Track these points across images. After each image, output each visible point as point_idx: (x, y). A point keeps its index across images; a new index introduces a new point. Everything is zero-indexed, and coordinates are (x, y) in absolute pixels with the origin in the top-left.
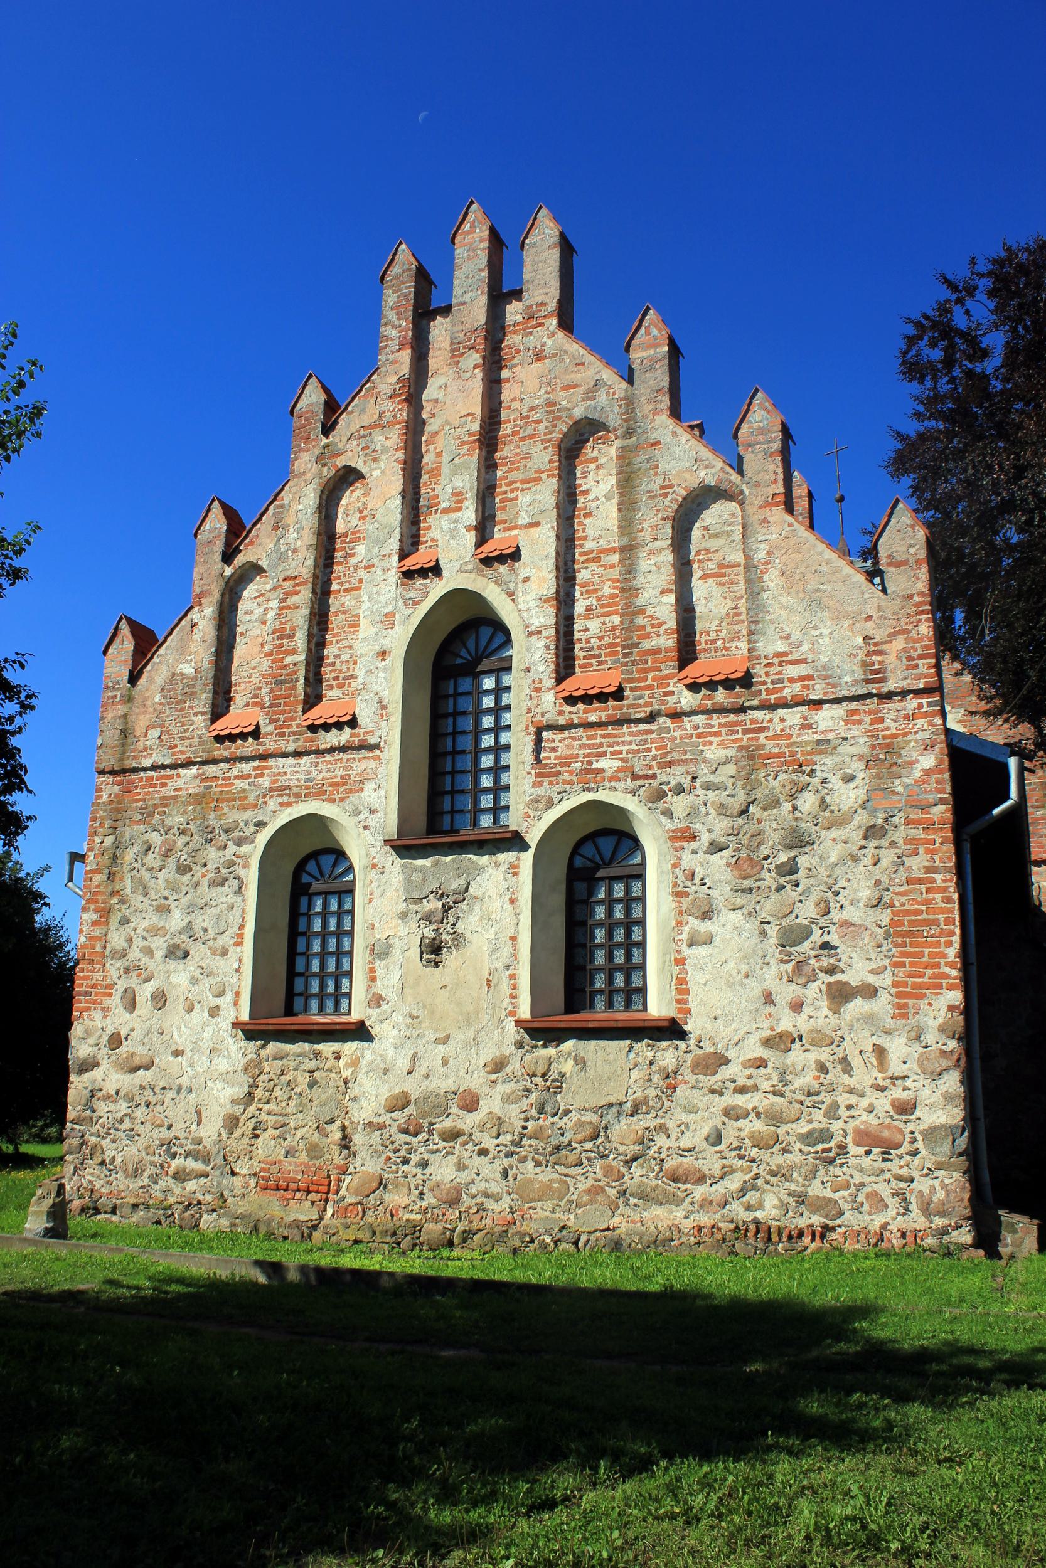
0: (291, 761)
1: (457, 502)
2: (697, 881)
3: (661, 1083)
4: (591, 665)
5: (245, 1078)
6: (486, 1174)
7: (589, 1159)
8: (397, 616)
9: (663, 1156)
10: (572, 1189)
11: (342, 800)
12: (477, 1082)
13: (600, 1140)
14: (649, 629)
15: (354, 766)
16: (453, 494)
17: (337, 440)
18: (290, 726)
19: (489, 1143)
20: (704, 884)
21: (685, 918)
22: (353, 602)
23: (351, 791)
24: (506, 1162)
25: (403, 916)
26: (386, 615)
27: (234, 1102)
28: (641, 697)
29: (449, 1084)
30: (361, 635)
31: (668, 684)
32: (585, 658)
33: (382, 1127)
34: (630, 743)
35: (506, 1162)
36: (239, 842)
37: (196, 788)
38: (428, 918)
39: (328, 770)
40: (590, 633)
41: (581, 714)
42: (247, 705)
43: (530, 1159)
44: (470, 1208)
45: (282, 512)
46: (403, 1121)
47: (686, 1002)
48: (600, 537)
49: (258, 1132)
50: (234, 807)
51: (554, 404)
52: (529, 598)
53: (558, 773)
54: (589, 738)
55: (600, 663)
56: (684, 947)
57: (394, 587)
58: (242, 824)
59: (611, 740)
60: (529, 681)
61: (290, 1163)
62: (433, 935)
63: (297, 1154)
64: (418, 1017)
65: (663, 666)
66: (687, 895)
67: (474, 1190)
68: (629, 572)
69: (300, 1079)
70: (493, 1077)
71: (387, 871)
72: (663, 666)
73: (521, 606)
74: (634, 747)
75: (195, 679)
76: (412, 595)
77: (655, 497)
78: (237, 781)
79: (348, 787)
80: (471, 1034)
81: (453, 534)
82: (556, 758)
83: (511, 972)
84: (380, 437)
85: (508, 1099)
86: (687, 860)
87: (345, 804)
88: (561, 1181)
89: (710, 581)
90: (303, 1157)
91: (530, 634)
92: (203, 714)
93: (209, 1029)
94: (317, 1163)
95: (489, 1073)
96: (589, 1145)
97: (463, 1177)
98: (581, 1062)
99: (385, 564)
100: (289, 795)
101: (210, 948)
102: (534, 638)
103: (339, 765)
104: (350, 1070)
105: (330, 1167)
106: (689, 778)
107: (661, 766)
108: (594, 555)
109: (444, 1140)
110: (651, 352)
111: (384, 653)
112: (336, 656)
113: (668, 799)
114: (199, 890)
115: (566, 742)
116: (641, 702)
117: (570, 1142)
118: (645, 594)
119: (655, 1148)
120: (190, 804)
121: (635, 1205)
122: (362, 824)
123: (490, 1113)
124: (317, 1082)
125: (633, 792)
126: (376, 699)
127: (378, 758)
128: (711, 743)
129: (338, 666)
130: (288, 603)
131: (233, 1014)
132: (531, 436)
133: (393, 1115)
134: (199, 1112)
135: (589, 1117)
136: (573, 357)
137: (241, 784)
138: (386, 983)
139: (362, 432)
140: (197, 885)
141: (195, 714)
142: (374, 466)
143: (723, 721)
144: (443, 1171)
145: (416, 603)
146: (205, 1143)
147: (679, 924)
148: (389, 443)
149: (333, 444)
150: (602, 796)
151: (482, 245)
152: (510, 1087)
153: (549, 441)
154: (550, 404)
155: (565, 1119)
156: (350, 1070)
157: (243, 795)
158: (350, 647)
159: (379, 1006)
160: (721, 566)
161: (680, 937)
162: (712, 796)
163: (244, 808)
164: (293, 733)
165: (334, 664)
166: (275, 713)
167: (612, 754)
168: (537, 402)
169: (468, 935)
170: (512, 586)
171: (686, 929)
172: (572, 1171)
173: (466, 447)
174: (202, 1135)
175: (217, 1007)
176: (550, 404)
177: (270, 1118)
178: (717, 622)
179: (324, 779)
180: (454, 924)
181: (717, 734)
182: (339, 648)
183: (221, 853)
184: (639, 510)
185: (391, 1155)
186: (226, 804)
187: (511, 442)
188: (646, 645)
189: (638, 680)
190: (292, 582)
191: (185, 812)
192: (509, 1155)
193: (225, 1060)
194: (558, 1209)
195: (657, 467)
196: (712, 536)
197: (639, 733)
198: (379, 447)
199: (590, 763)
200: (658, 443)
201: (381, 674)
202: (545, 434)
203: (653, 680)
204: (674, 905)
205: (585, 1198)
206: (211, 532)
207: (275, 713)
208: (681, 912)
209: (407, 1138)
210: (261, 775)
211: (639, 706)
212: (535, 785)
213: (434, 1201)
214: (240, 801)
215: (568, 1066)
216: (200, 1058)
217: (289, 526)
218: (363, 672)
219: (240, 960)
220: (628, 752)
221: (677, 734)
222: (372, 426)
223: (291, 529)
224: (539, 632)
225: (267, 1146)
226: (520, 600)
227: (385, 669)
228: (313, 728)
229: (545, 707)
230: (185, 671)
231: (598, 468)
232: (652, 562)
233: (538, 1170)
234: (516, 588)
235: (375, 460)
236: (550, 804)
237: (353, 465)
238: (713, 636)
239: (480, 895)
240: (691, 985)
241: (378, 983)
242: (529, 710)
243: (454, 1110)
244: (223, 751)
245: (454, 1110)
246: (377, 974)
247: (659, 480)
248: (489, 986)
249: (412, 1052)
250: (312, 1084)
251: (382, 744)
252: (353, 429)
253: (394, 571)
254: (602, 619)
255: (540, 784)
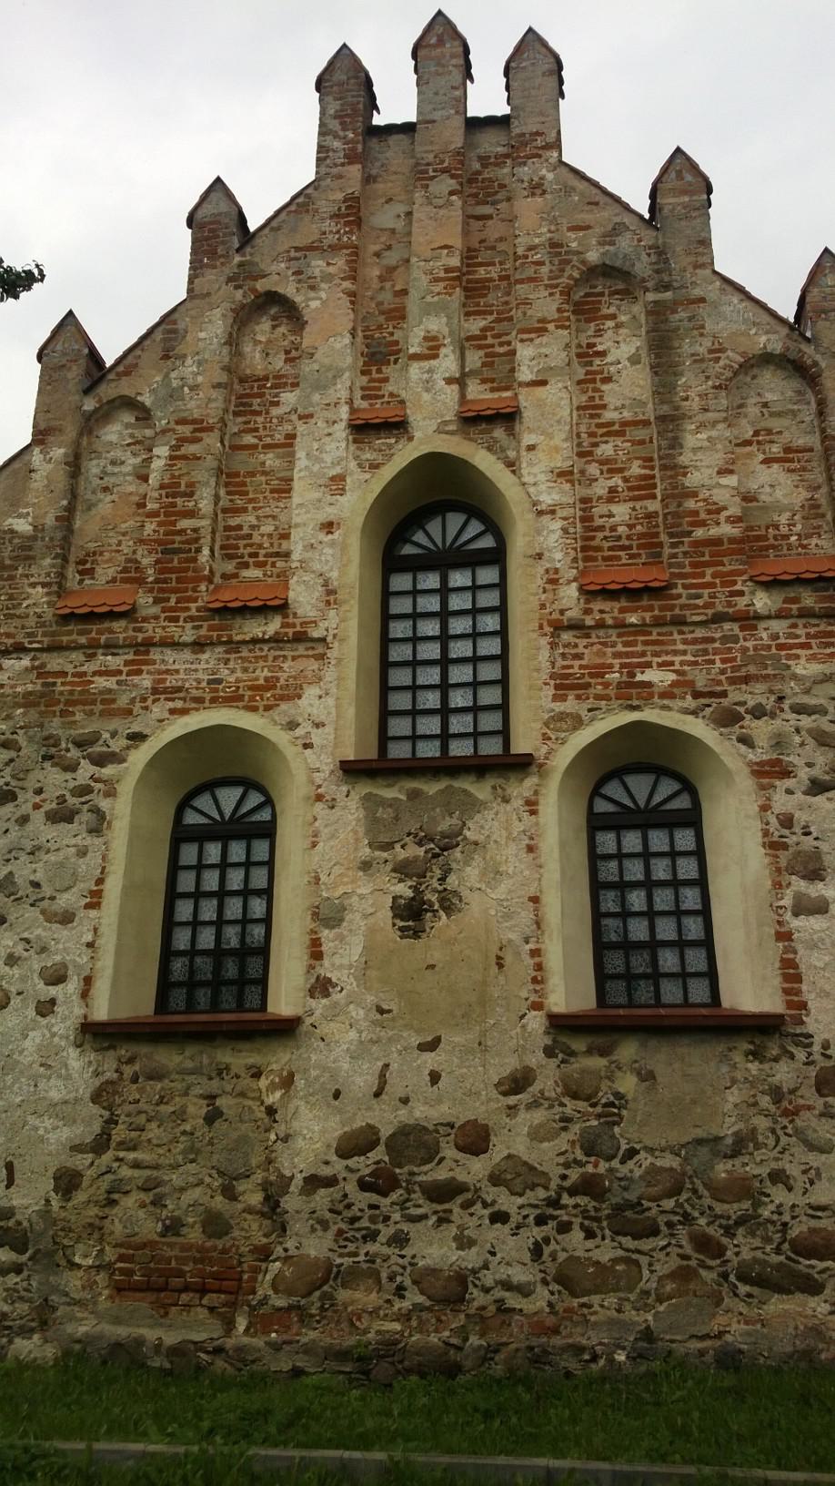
0: (187, 655)
1: (430, 348)
2: (797, 829)
3: (773, 1108)
4: (619, 558)
5: (96, 1110)
6: (508, 1257)
7: (670, 1225)
8: (348, 480)
9: (786, 1218)
10: (646, 1273)
11: (268, 708)
12: (486, 1106)
13: (684, 1196)
14: (703, 516)
15: (285, 666)
16: (425, 339)
17: (257, 259)
18: (188, 609)
19: (507, 1202)
20: (808, 834)
21: (786, 878)
22: (277, 463)
23: (282, 698)
24: (538, 1233)
25: (366, 866)
26: (333, 479)
27: (77, 1149)
28: (699, 597)
29: (443, 1112)
30: (296, 499)
31: (735, 583)
32: (610, 549)
33: (331, 1182)
34: (684, 653)
35: (538, 1233)
36: (100, 761)
37: (32, 686)
38: (403, 870)
39: (245, 670)
40: (617, 519)
41: (616, 614)
42: (114, 580)
43: (576, 1227)
44: (483, 1308)
45: (175, 339)
46: (367, 1171)
47: (798, 992)
48: (623, 406)
49: (115, 1196)
50: (91, 713)
51: (561, 246)
52: (535, 470)
53: (588, 686)
54: (626, 644)
55: (631, 557)
56: (788, 916)
57: (343, 445)
58: (106, 735)
59: (657, 648)
60: (541, 571)
61: (171, 1245)
62: (410, 893)
63: (184, 1230)
64: (389, 1011)
65: (725, 560)
66: (785, 847)
67: (488, 1278)
68: (672, 447)
69: (191, 1109)
70: (512, 1100)
71: (340, 804)
72: (725, 560)
73: (526, 479)
74: (689, 658)
75: (34, 538)
76: (368, 456)
77: (702, 360)
78: (96, 678)
79: (278, 691)
80: (472, 1036)
81: (428, 385)
82: (581, 667)
83: (531, 946)
84: (320, 262)
85: (536, 1135)
86: (781, 802)
87: (275, 714)
88: (627, 1261)
89: (776, 466)
90: (194, 1235)
91: (540, 513)
92: (44, 585)
93: (35, 1037)
94: (220, 1244)
95: (505, 1094)
96: (669, 1204)
97: (471, 1258)
98: (647, 1077)
99: (330, 415)
100: (184, 699)
101: (43, 912)
102: (546, 519)
103: (262, 663)
104: (278, 1094)
105: (244, 1249)
106: (773, 698)
107: (732, 681)
108: (616, 427)
109: (432, 1200)
110: (686, 199)
111: (330, 524)
112: (253, 527)
113: (746, 723)
114: (30, 827)
115: (595, 648)
116: (700, 602)
117: (640, 1198)
118: (697, 474)
119: (772, 1207)
120: (18, 705)
121: (749, 1295)
122: (300, 742)
123: (509, 1157)
124: (221, 1114)
125: (694, 713)
126: (321, 581)
127: (321, 657)
128: (798, 657)
129: (256, 539)
130: (183, 451)
131: (78, 1011)
132: (531, 280)
133: (350, 1162)
134: (10, 1167)
135: (669, 1161)
136: (582, 195)
137: (102, 683)
138: (337, 960)
139: (293, 254)
140: (24, 820)
141: (33, 585)
142: (312, 294)
143: (812, 631)
144: (435, 1250)
145: (375, 466)
146: (18, 1217)
147: (778, 885)
148: (331, 269)
149: (250, 263)
150: (650, 715)
151: (454, 61)
152: (539, 1116)
153: (556, 286)
154: (554, 245)
155: (631, 1164)
156: (278, 1094)
157: (108, 698)
158: (274, 517)
159: (327, 995)
160: (787, 450)
161: (781, 903)
162: (806, 721)
163: (108, 714)
164: (192, 619)
165: (250, 536)
166: (161, 590)
167: (659, 665)
168: (537, 241)
169: (465, 893)
170: (512, 454)
171: (789, 893)
172: (646, 1244)
173: (442, 284)
174: (14, 1203)
175: (53, 1002)
176: (554, 245)
177: (137, 1173)
178: (788, 514)
179: (238, 681)
180: (442, 880)
181: (807, 646)
182: (258, 518)
183: (69, 776)
184: (682, 375)
185: (344, 1226)
186: (80, 707)
187: (497, 287)
188: (699, 533)
189: (694, 576)
190: (191, 427)
191: (8, 717)
192: (541, 1221)
193: (60, 1083)
194: (627, 1306)
195: (703, 327)
196: (772, 415)
197: (695, 641)
198: (317, 272)
199: (632, 675)
200: (702, 300)
201: (328, 551)
202: (550, 278)
203: (714, 575)
204: (767, 860)
205: (670, 1287)
206: (64, 354)
207: (161, 590)
208: (779, 870)
209: (373, 1198)
210: (139, 672)
211: (697, 607)
212: (555, 698)
213: (421, 1299)
214: (107, 706)
215: (628, 1084)
216: (16, 1081)
217: (185, 356)
218: (300, 547)
219: (95, 930)
220: (682, 663)
221: (749, 644)
222: (310, 248)
223: (189, 361)
224: (553, 512)
225: (132, 1217)
226: (524, 472)
227: (332, 544)
228: (225, 611)
229: (565, 603)
230: (16, 528)
231: (618, 326)
232: (703, 436)
233: (590, 1244)
234: (518, 458)
235: (313, 288)
236: (578, 723)
237: (281, 291)
238: (784, 530)
239: (481, 838)
240: (803, 968)
241: (326, 962)
242: (543, 606)
243: (449, 1152)
244: (73, 634)
245: (449, 1152)
246: (324, 948)
247: (707, 343)
248: (500, 966)
249: (380, 1064)
250: (213, 1117)
251: (329, 639)
252: (281, 249)
253: (343, 424)
254: (631, 504)
255: (563, 698)
